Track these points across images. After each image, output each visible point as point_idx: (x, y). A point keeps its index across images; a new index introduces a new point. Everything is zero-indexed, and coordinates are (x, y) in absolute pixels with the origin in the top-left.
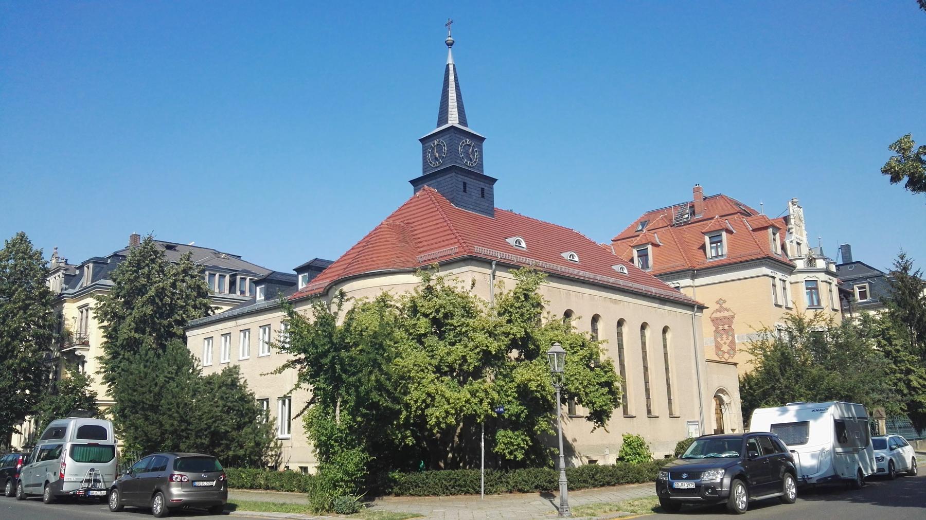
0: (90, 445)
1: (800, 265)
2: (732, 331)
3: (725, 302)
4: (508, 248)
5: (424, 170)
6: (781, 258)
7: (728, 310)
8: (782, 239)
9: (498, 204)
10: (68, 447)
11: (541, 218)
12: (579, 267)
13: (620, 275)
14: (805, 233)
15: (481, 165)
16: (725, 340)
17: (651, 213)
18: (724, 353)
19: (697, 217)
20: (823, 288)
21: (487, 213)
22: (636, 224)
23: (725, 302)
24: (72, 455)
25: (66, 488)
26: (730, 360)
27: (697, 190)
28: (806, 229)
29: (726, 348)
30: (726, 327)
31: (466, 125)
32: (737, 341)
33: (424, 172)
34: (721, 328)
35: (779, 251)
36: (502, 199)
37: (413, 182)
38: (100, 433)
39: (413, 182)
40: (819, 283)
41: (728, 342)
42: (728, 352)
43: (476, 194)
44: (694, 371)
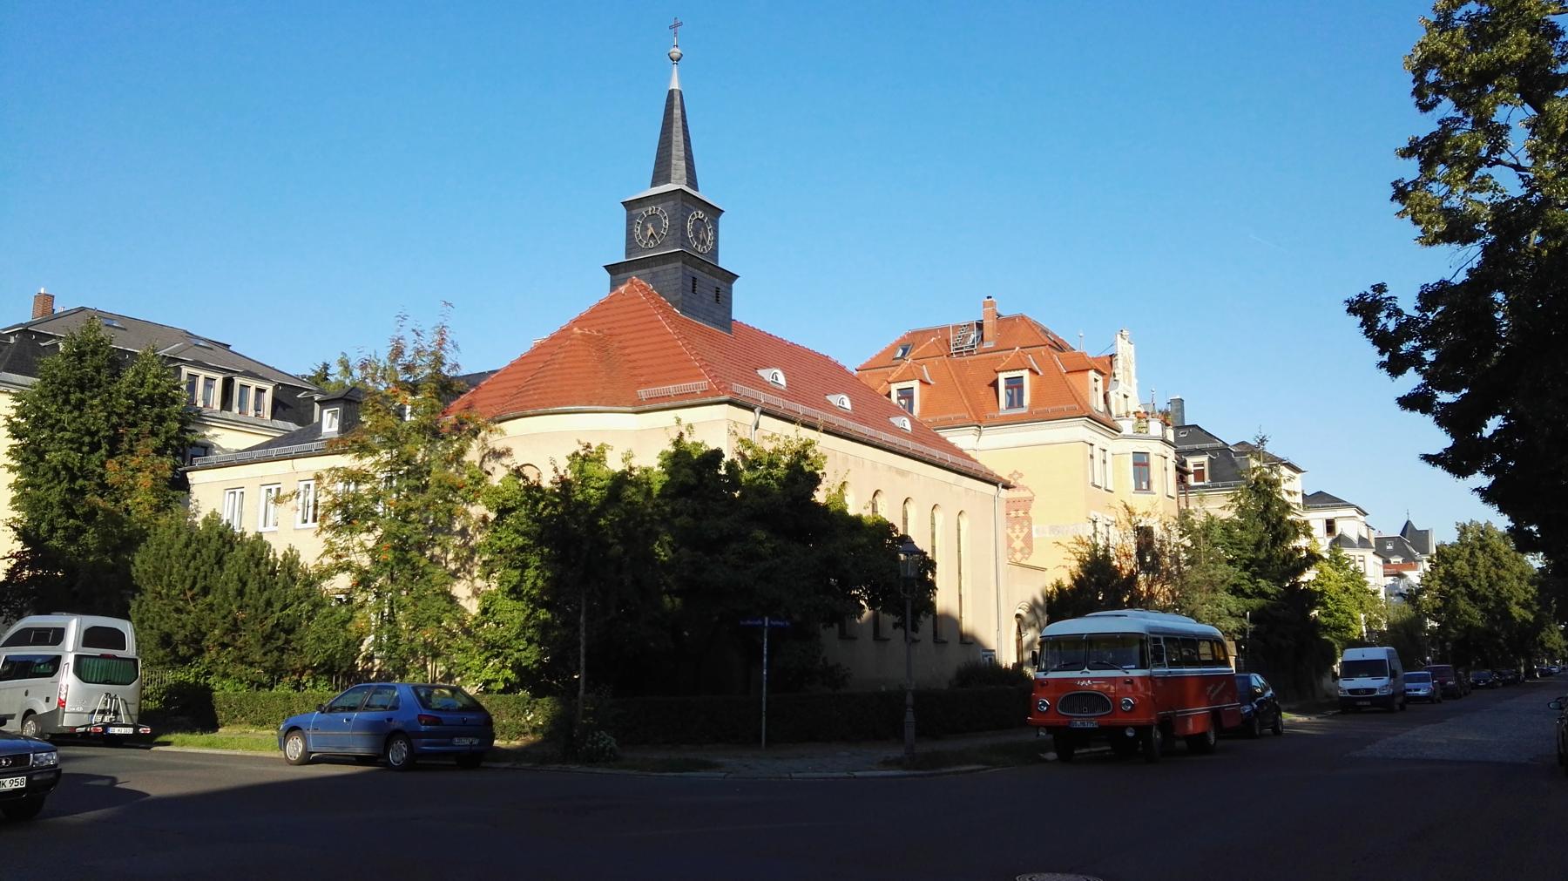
0: (102, 656)
1: (1127, 426)
2: (1029, 520)
3: (1021, 475)
4: (829, 407)
5: (630, 249)
6: (1103, 417)
7: (1025, 488)
8: (1105, 387)
9: (739, 313)
10: (69, 659)
11: (790, 336)
12: (782, 394)
13: (899, 432)
14: (1135, 381)
15: (714, 253)
16: (1019, 532)
17: (915, 333)
18: (1015, 550)
19: (987, 345)
20: (1155, 464)
21: (715, 323)
22: (893, 348)
23: (1021, 475)
24: (79, 671)
25: (67, 721)
26: (1024, 562)
27: (989, 301)
28: (1137, 376)
29: (1018, 544)
30: (1021, 513)
31: (695, 188)
32: (1035, 535)
33: (628, 254)
34: (1013, 514)
35: (1101, 407)
36: (746, 307)
37: (611, 269)
38: (116, 639)
39: (611, 269)
40: (1152, 457)
41: (1022, 535)
42: (1021, 550)
43: (709, 296)
44: (993, 578)
